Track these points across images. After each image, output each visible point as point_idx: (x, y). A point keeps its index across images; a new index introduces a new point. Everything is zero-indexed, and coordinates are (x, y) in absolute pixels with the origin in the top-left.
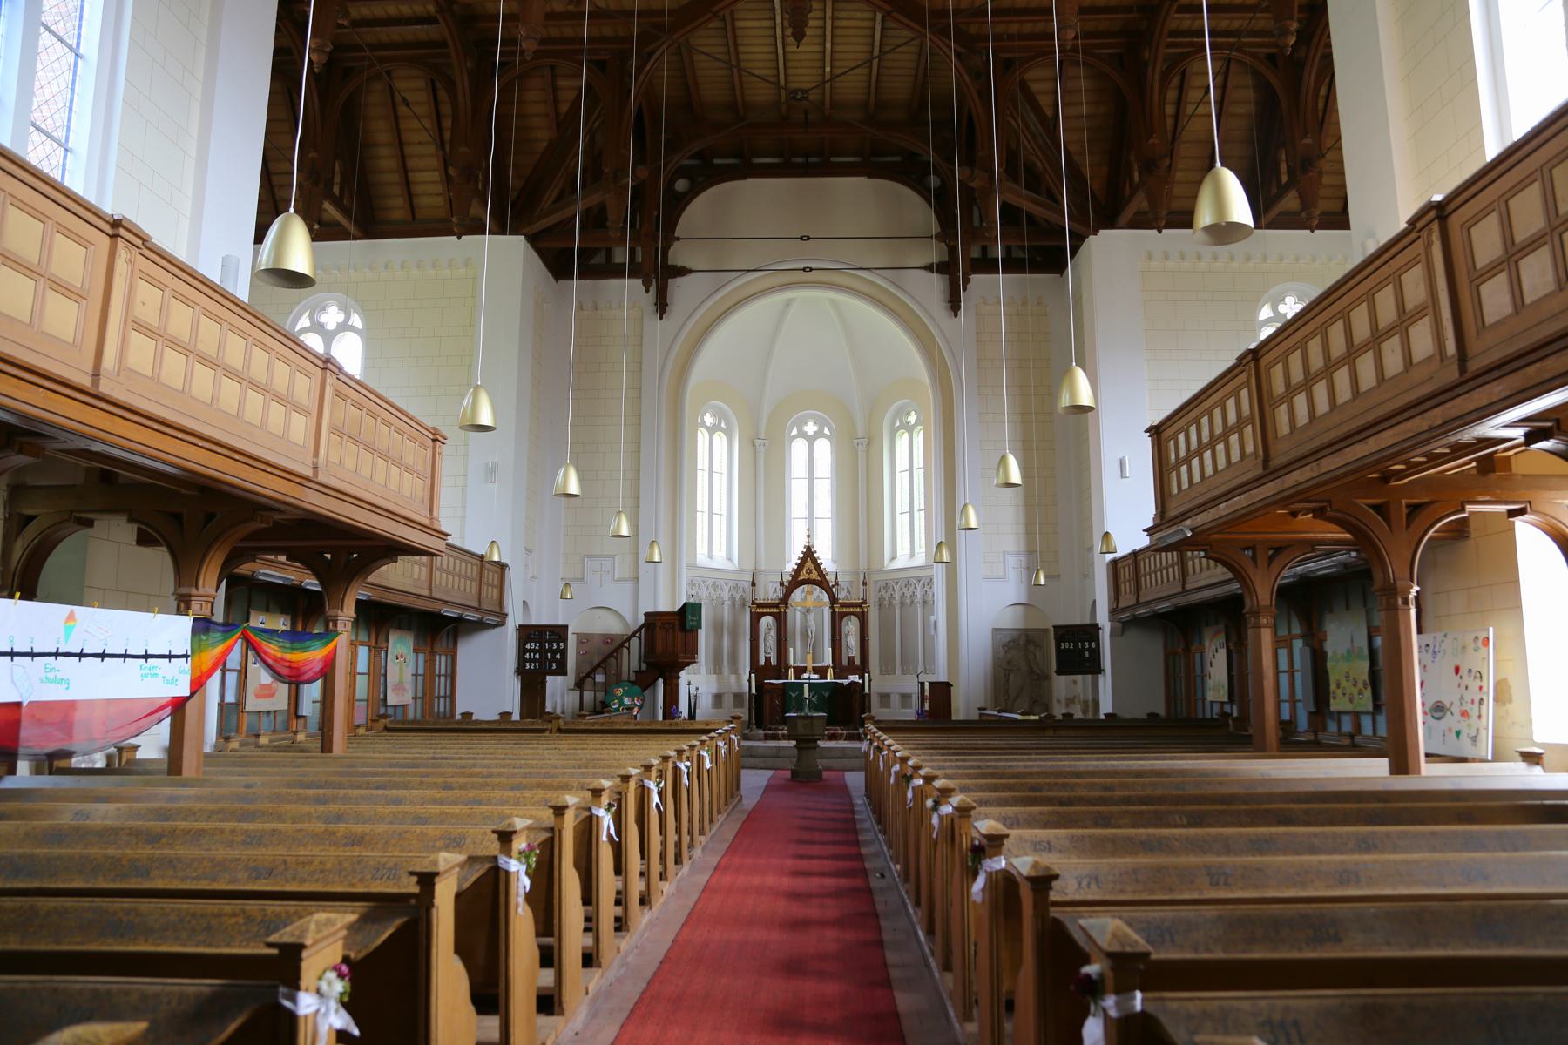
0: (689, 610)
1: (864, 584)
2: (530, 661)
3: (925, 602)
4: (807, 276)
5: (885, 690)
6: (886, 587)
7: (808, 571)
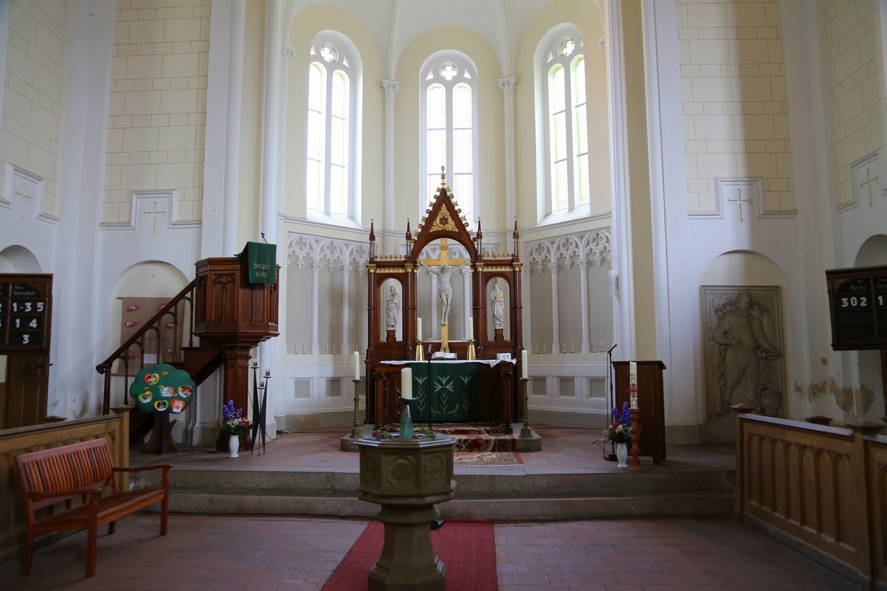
1: (516, 235)
5: (568, 373)
6: (540, 248)
7: (444, 214)
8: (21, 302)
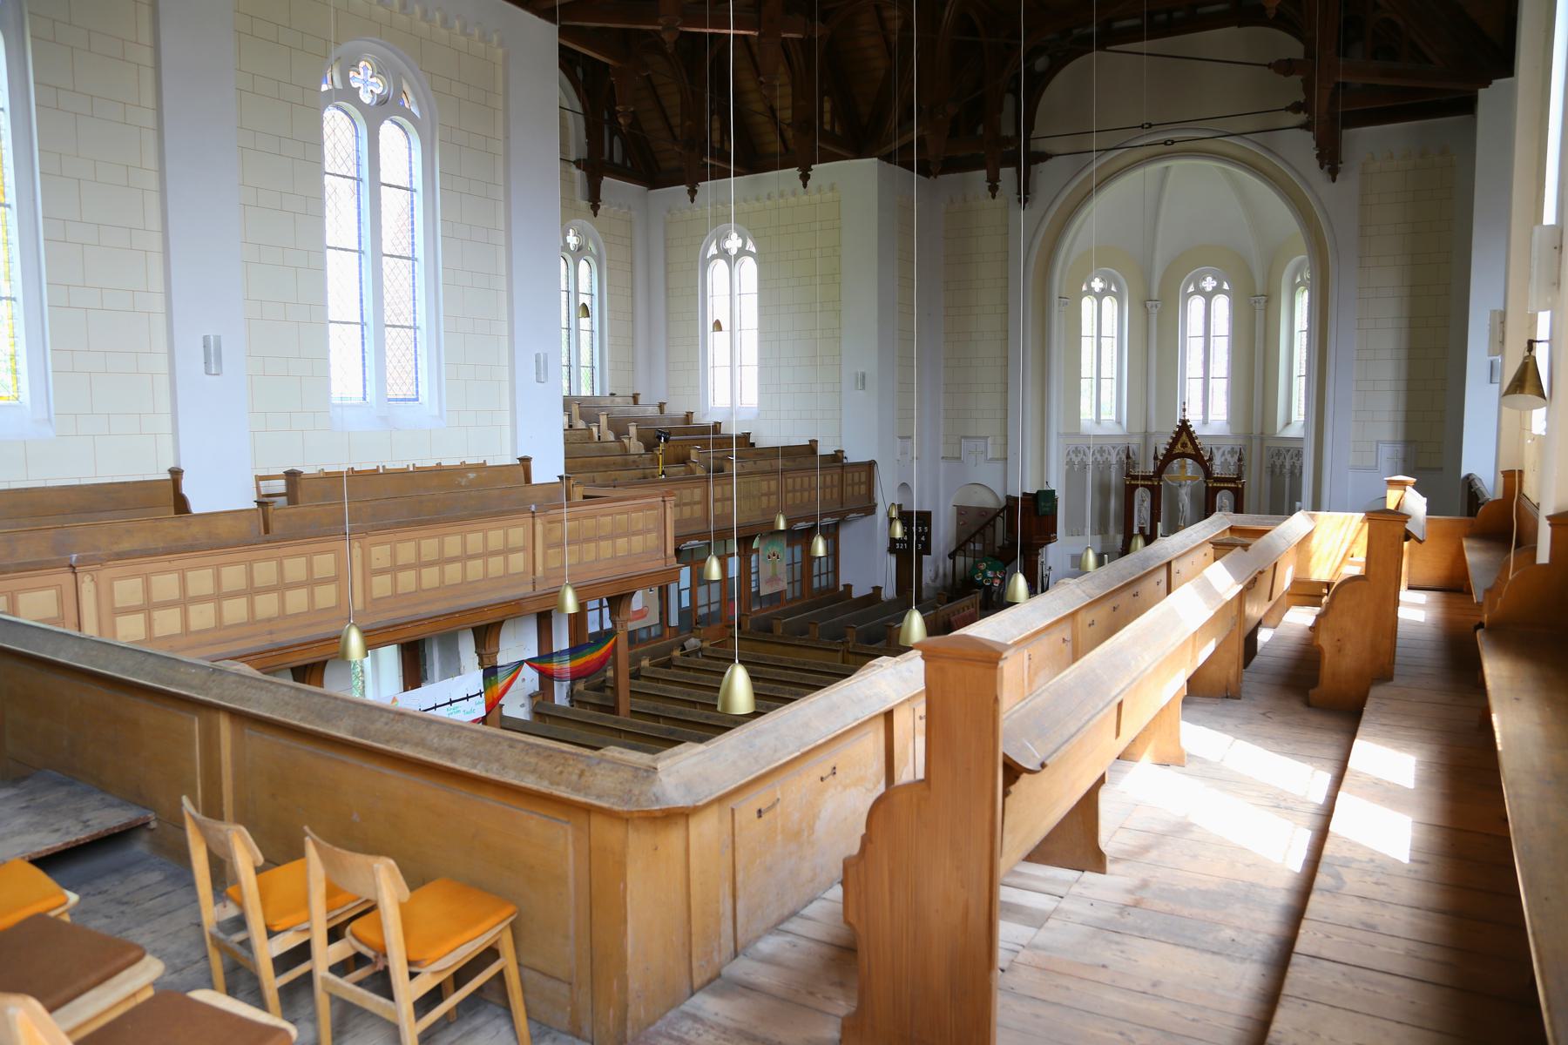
3: (1292, 473)
4: (1170, 149)
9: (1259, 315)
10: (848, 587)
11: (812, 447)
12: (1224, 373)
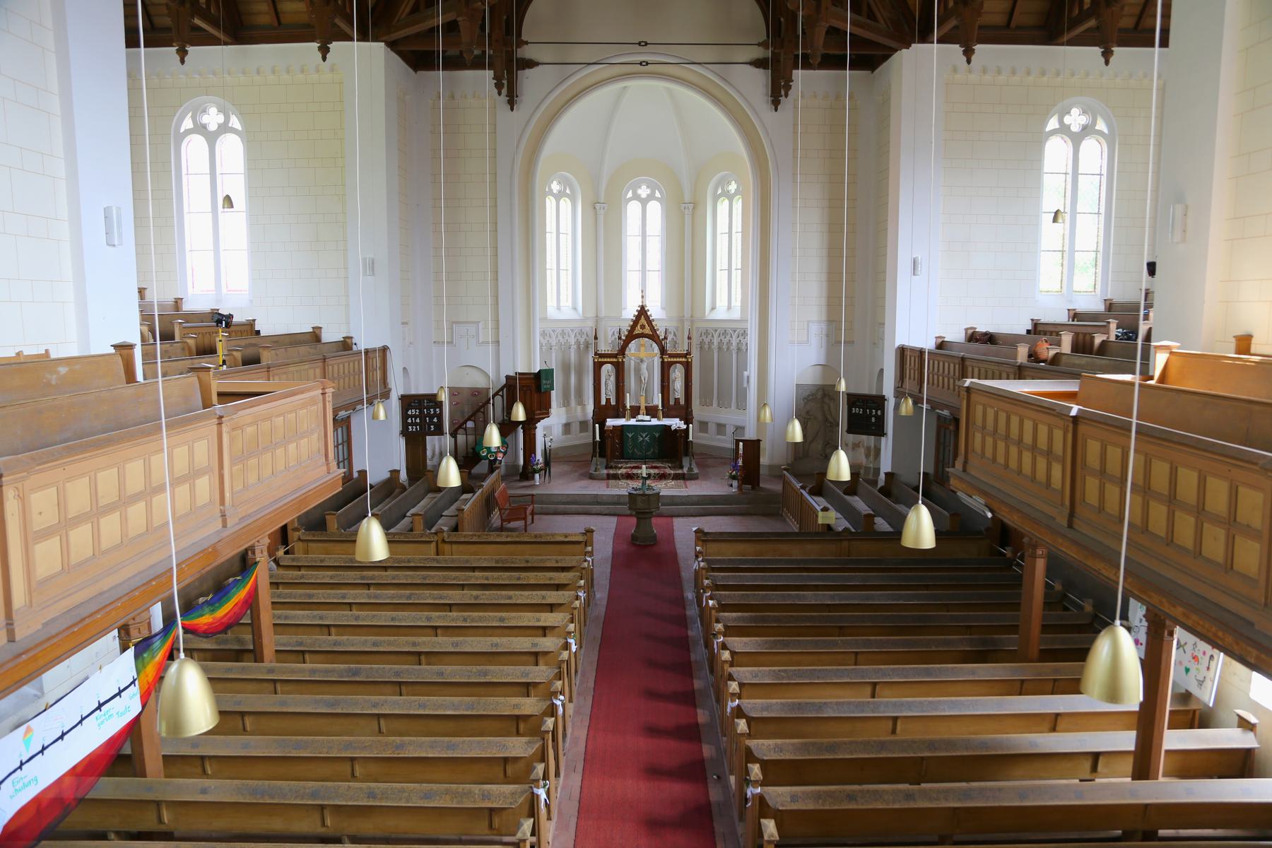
0: (543, 376)
1: (689, 338)
2: (412, 424)
3: (739, 349)
4: (644, 69)
5: (722, 422)
8: (428, 409)
9: (688, 219)
10: (363, 473)
11: (315, 336)
12: (658, 267)
